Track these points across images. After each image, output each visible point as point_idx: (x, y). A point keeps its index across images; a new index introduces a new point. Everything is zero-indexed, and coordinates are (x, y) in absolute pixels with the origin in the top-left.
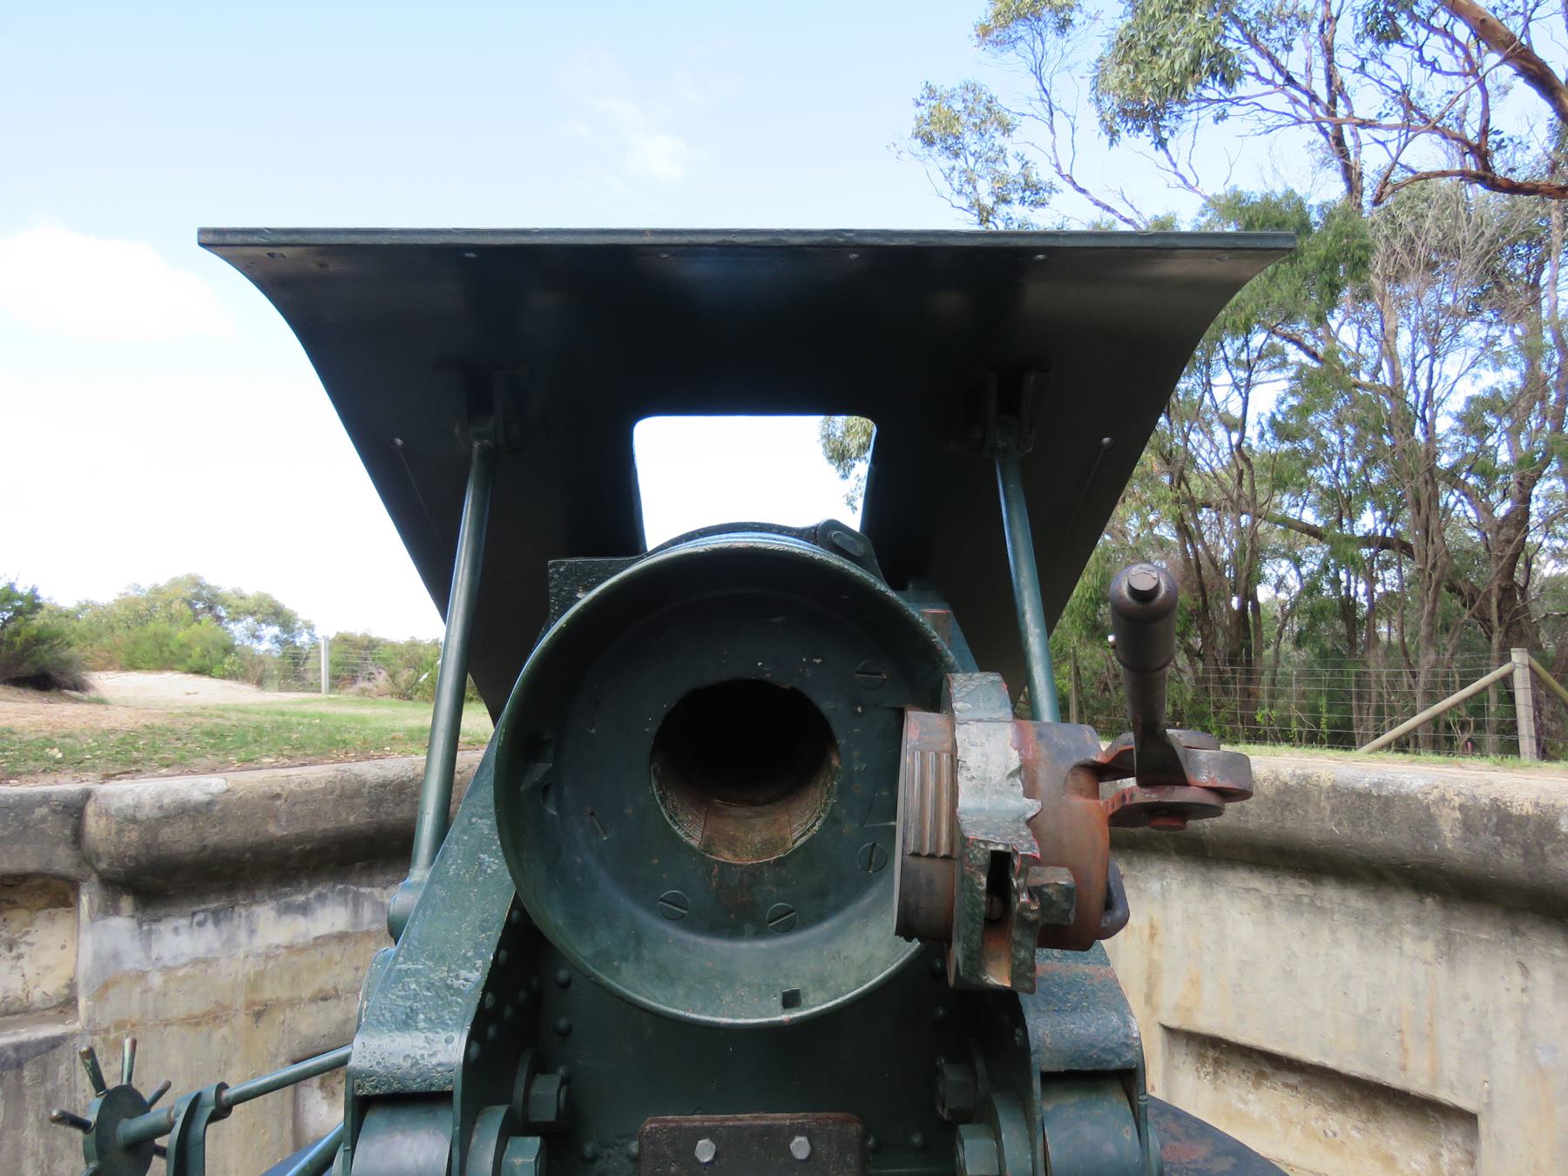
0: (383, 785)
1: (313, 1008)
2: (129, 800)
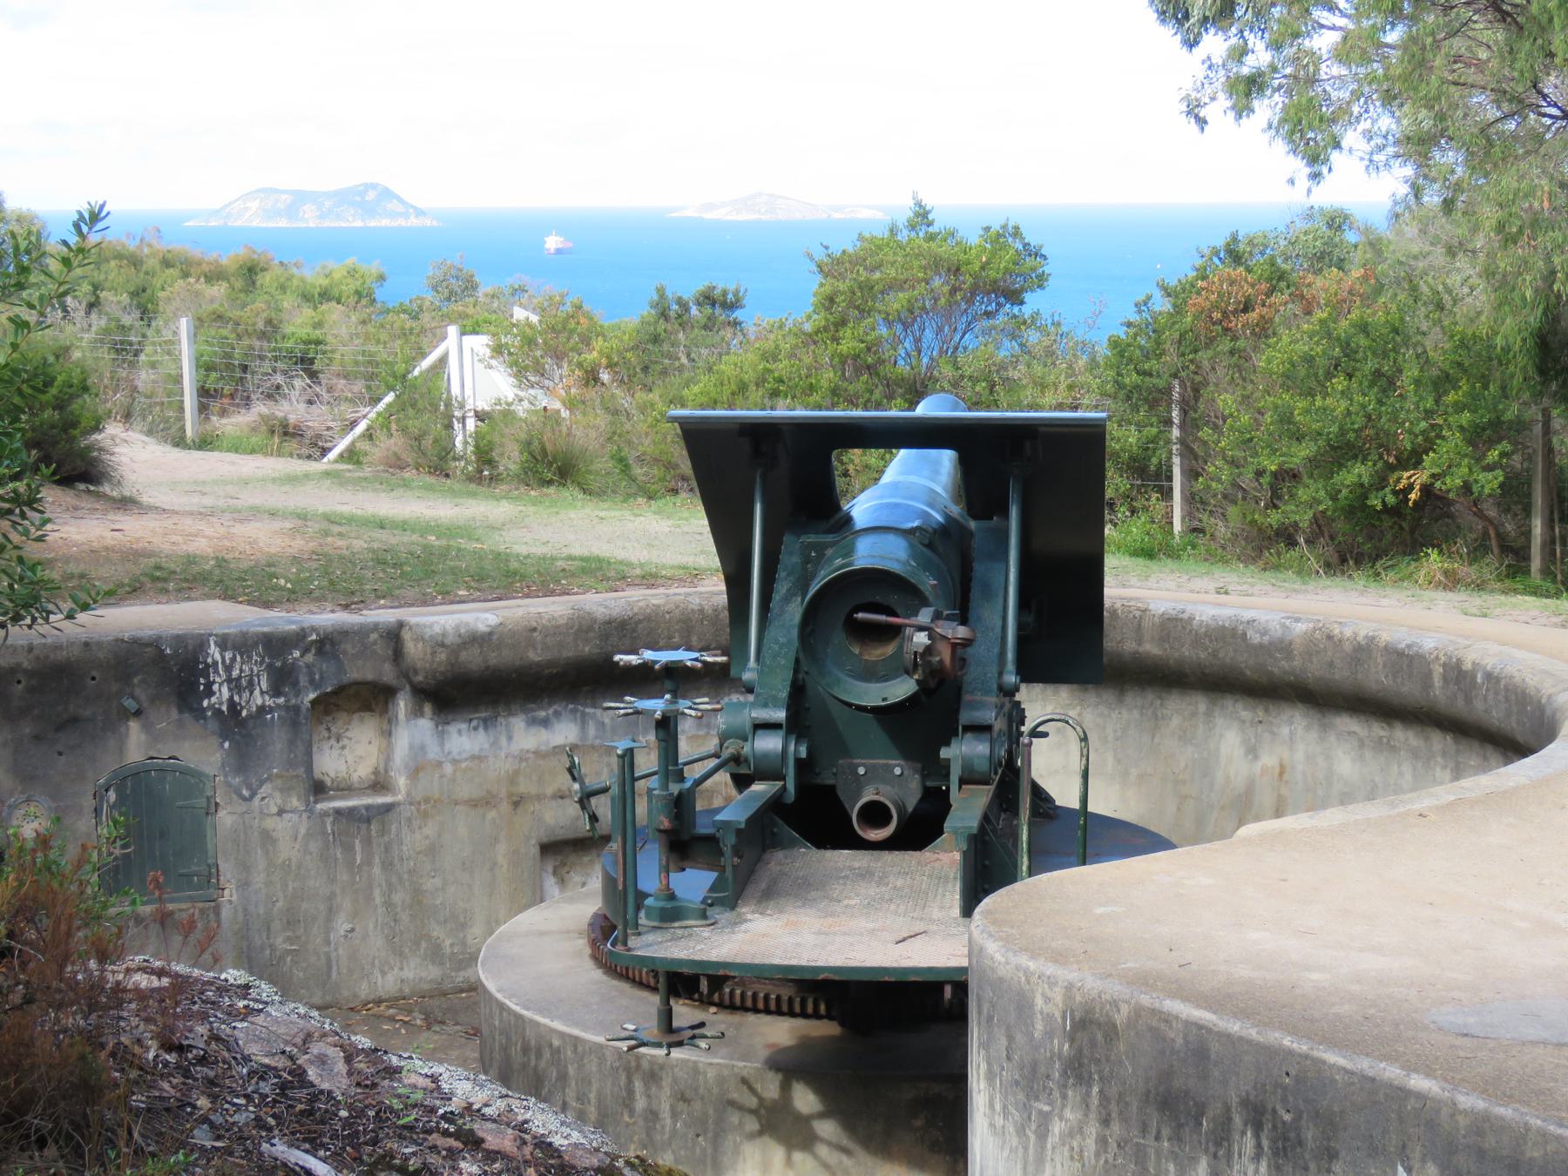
0: (609, 622)
1: (554, 804)
2: (437, 629)
